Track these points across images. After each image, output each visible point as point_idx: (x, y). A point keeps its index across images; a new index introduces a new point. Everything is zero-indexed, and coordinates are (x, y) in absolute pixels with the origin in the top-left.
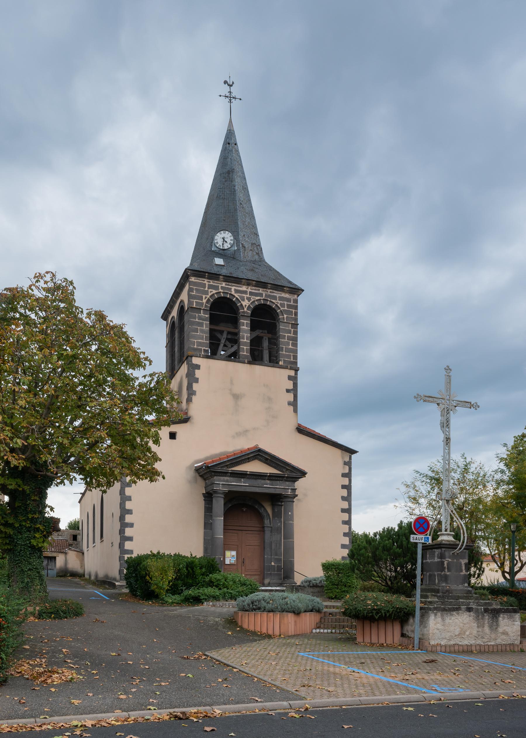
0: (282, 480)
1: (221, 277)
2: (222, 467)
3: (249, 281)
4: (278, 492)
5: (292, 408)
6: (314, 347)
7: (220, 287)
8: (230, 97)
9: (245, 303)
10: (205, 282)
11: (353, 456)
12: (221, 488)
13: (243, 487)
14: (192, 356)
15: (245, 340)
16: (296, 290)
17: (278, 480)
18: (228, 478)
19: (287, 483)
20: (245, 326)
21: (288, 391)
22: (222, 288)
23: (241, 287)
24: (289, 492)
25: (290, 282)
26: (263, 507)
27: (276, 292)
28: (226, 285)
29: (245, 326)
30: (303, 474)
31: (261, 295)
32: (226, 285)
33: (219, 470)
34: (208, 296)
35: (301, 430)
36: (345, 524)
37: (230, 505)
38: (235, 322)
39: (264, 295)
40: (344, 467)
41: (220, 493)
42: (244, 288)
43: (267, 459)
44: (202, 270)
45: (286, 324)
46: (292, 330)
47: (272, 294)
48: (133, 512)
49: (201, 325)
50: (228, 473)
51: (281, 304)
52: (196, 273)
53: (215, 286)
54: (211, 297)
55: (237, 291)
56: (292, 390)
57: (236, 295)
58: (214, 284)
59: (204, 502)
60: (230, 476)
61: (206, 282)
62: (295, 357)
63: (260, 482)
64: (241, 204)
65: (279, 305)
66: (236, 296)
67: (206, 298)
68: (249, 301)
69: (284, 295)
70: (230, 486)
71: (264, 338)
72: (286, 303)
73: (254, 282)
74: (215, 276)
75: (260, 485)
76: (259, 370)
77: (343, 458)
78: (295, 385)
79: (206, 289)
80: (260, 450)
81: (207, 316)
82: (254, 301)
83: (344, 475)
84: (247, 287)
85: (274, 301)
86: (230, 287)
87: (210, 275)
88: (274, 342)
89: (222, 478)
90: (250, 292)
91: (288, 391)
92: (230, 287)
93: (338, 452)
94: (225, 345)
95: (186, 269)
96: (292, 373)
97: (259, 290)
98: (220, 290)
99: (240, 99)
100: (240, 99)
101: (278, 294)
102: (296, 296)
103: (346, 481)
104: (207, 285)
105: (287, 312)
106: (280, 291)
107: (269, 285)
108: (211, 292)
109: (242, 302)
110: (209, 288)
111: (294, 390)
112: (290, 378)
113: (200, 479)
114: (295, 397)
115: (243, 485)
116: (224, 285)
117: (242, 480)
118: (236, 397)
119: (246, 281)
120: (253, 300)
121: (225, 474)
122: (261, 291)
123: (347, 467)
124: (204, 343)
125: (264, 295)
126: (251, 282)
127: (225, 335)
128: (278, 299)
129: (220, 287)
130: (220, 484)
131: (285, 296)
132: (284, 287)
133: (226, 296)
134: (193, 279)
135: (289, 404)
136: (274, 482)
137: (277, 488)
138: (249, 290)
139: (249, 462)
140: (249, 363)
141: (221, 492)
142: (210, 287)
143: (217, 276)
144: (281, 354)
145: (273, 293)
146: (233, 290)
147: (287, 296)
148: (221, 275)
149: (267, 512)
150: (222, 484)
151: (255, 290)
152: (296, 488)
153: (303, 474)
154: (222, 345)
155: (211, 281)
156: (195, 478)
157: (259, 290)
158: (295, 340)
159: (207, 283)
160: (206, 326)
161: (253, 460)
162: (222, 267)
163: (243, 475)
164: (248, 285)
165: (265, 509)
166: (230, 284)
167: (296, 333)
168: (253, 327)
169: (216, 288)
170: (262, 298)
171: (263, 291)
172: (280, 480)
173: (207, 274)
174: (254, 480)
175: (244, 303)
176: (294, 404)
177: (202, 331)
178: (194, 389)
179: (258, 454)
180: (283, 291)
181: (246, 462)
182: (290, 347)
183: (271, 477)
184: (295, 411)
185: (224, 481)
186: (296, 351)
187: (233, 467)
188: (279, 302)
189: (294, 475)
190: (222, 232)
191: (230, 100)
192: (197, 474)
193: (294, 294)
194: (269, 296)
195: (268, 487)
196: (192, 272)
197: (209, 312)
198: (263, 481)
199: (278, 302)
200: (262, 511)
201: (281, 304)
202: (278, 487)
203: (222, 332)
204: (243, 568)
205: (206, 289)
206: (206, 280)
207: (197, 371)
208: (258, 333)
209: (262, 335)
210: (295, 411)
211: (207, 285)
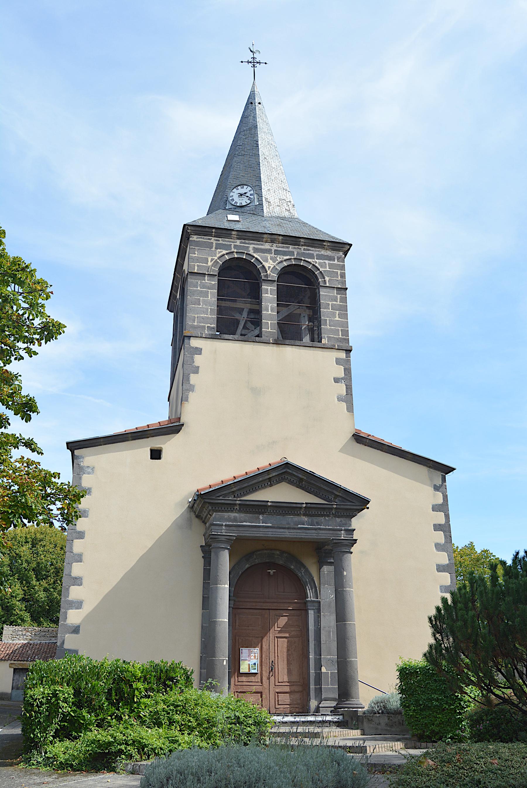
0: (328, 516)
1: (233, 233)
2: (225, 495)
3: (273, 237)
4: (323, 535)
5: (344, 405)
6: (366, 301)
7: (232, 246)
8: (254, 62)
9: (269, 264)
10: (211, 241)
11: (448, 477)
12: (224, 531)
13: (261, 530)
14: (189, 337)
15: (270, 312)
16: (341, 245)
17: (322, 516)
18: (236, 515)
19: (338, 520)
20: (269, 295)
21: (336, 380)
22: (235, 246)
23: (262, 245)
24: (343, 535)
25: (332, 237)
26: (304, 567)
27: (313, 249)
28: (241, 243)
29: (269, 295)
30: (362, 503)
31: (292, 253)
32: (241, 243)
33: (221, 500)
34: (216, 258)
35: (359, 438)
36: (197, 348)
37: (247, 566)
38: (256, 295)
39: (295, 253)
40: (434, 495)
41: (221, 542)
42: (267, 246)
43: (301, 480)
44: (208, 225)
45: (328, 290)
46: (339, 296)
47: (307, 252)
48: (84, 581)
49: (206, 294)
50: (235, 504)
51: (319, 263)
52: (200, 229)
53: (225, 244)
54: (219, 258)
55: (256, 250)
56: (342, 379)
57: (256, 255)
58: (224, 243)
59: (202, 560)
60: (240, 511)
61: (213, 240)
62: (346, 333)
63: (291, 519)
64: (265, 158)
65: (317, 265)
66: (256, 256)
67: (212, 260)
68: (274, 262)
69: (323, 252)
70: (241, 529)
71: (302, 315)
72: (327, 262)
73: (281, 238)
74: (224, 232)
75: (292, 525)
76: (289, 352)
77: (431, 479)
78: (348, 371)
79: (214, 249)
80: (287, 465)
81: (213, 283)
82: (281, 262)
83: (436, 508)
84: (270, 244)
85: (309, 260)
86: (246, 245)
87: (219, 231)
88: (315, 317)
89: (226, 515)
90: (275, 250)
91: (336, 380)
92: (246, 245)
93: (423, 470)
94: (245, 327)
95: (185, 225)
96: (342, 355)
97: (288, 248)
98: (233, 250)
99: (266, 63)
100: (266, 63)
101: (315, 251)
102: (341, 253)
103: (440, 518)
104: (214, 244)
105: (329, 273)
106: (319, 247)
107: (302, 240)
108: (219, 252)
109: (264, 263)
110: (216, 248)
111: (347, 378)
112: (338, 361)
113: (196, 521)
114: (349, 388)
115: (263, 526)
116: (238, 242)
117: (261, 517)
118: (256, 391)
119: (269, 236)
120: (279, 260)
121: (230, 507)
122: (291, 248)
123: (440, 495)
124: (208, 318)
125: (295, 253)
126: (276, 237)
127: (245, 314)
128: (319, 262)
129: (232, 246)
130: (222, 525)
131: (326, 254)
132: (324, 241)
133: (241, 256)
134: (194, 238)
135: (340, 399)
136: (316, 519)
137: (320, 529)
138: (274, 248)
139: (271, 485)
140: (277, 343)
141: (223, 538)
142: (218, 247)
143: (229, 232)
144: (324, 328)
145: (309, 250)
146: (251, 249)
147: (329, 253)
148: (233, 230)
149: (310, 575)
150: (226, 522)
151: (283, 247)
152: (353, 527)
153: (362, 503)
154: (241, 326)
155: (220, 239)
156: (190, 520)
157: (288, 248)
158: (343, 310)
159: (215, 242)
160: (212, 296)
161: (278, 482)
162: (237, 223)
163: (261, 508)
164: (272, 241)
165: (307, 571)
166: (247, 241)
167: (344, 300)
168: (282, 297)
169: (227, 247)
170: (293, 257)
171: (295, 248)
172: (324, 516)
173: (214, 230)
174: (281, 517)
175: (266, 265)
176: (348, 398)
177: (205, 303)
178: (192, 382)
179: (287, 473)
180: (323, 247)
181: (265, 487)
182: (337, 319)
183: (309, 510)
184: (350, 409)
185: (229, 520)
186: (346, 325)
187: (245, 495)
188: (317, 261)
189: (348, 505)
190: (239, 187)
191: (254, 65)
192: (192, 514)
193: (339, 250)
194: (304, 254)
195: (303, 528)
196: (193, 228)
197: (216, 278)
198: (296, 519)
199: (317, 262)
200: (301, 573)
201: (319, 263)
202: (325, 528)
203: (241, 311)
204: (272, 679)
205: (214, 249)
206: (213, 238)
207: (197, 357)
208: (293, 307)
209: (298, 311)
210: (350, 409)
211: (214, 244)
